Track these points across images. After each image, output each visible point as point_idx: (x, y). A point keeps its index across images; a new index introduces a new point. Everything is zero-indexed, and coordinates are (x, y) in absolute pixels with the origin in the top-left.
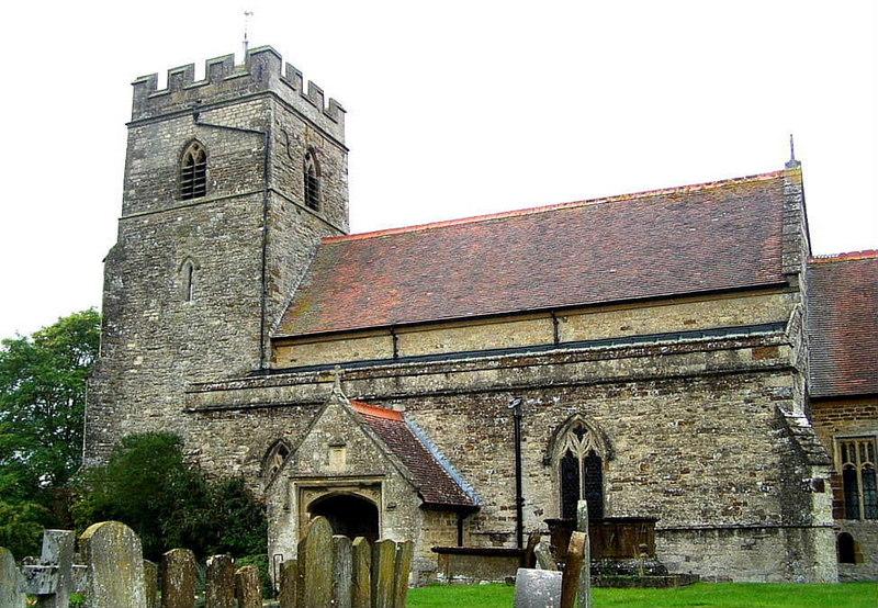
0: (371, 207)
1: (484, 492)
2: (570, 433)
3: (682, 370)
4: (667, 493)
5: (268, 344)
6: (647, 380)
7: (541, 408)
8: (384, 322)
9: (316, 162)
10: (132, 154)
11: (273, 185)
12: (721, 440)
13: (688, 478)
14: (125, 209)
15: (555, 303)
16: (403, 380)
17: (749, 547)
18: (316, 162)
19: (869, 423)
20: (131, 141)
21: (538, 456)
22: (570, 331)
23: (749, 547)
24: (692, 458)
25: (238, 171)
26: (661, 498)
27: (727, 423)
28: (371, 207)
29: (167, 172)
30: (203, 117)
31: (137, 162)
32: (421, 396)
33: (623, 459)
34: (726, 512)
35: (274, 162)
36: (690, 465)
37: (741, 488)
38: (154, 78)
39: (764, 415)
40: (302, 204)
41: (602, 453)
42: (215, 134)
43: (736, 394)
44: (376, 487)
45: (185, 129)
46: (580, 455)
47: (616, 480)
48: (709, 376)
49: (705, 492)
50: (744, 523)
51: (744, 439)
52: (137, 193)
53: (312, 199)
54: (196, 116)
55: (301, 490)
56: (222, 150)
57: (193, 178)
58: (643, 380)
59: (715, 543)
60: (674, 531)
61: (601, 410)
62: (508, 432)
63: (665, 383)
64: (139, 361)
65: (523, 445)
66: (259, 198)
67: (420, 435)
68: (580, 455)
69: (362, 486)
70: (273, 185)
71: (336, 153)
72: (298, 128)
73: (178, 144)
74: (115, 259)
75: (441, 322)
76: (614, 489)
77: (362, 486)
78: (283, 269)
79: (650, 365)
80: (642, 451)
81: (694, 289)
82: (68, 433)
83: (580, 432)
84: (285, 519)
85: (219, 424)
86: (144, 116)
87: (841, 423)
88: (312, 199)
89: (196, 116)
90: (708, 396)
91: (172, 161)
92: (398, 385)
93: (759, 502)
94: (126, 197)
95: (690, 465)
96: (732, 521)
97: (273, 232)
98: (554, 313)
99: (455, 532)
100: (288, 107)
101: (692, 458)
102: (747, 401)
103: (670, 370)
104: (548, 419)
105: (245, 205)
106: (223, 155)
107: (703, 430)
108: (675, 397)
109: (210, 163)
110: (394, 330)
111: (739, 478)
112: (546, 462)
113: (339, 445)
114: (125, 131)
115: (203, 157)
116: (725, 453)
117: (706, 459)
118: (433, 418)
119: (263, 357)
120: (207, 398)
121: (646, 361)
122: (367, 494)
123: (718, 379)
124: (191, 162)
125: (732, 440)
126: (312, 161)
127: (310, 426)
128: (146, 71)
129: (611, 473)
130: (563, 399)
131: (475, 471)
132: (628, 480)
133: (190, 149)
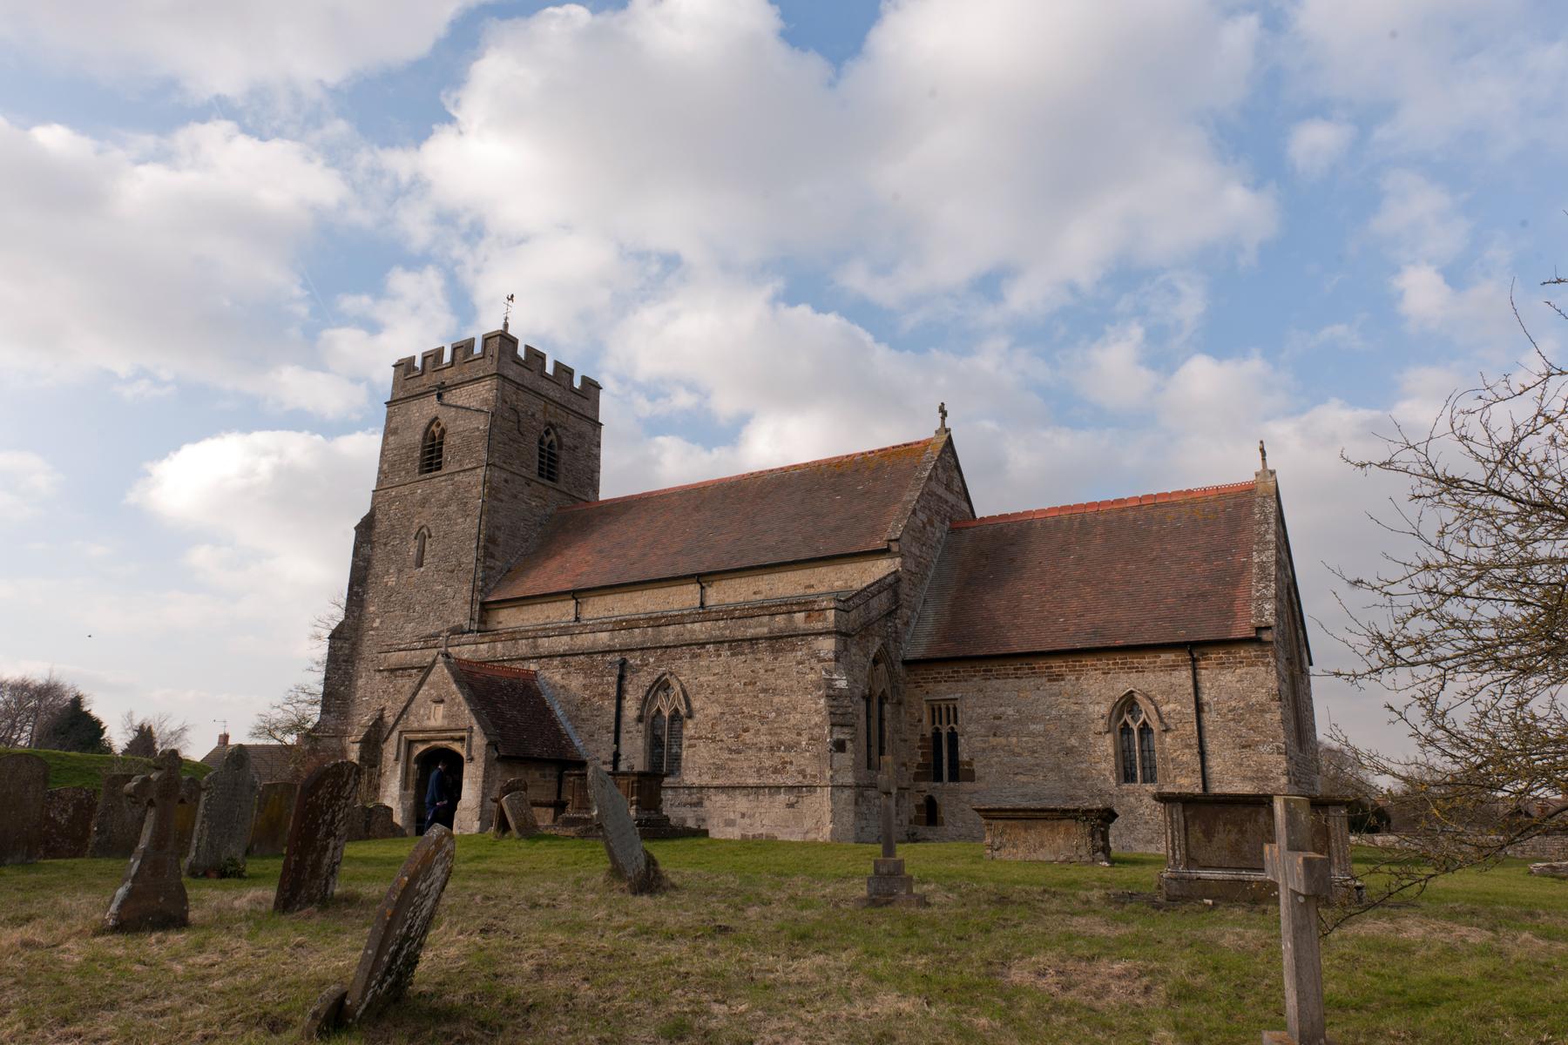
1: (592, 746)
3: (750, 633)
4: (730, 751)
8: (570, 587)
9: (559, 437)
13: (747, 737)
14: (380, 482)
15: (702, 569)
16: (540, 641)
17: (791, 806)
18: (559, 437)
19: (953, 685)
20: (389, 419)
23: (791, 806)
24: (752, 717)
26: (726, 755)
27: (782, 683)
29: (412, 449)
30: (447, 397)
31: (391, 439)
32: (550, 656)
34: (776, 771)
37: (789, 748)
38: (440, 352)
39: (812, 677)
40: (535, 476)
41: (683, 711)
42: (453, 412)
43: (790, 656)
45: (430, 407)
47: (692, 738)
48: (770, 638)
49: (760, 749)
51: (798, 697)
54: (440, 396)
58: (719, 642)
59: (765, 800)
60: (734, 788)
62: (613, 691)
63: (735, 645)
64: (377, 624)
69: (453, 739)
72: (537, 406)
73: (425, 422)
75: (660, 580)
76: (690, 746)
77: (453, 739)
79: (726, 628)
80: (714, 710)
81: (813, 554)
84: (394, 771)
85: (400, 681)
86: (401, 395)
87: (931, 686)
90: (768, 658)
91: (419, 437)
92: (536, 647)
93: (803, 761)
98: (702, 578)
99: (553, 785)
101: (752, 717)
102: (799, 663)
107: (765, 691)
108: (743, 658)
110: (577, 594)
111: (788, 737)
112: (640, 719)
114: (385, 409)
115: (443, 431)
116: (779, 712)
117: (763, 719)
118: (558, 677)
121: (721, 623)
122: (456, 747)
123: (779, 641)
125: (785, 700)
126: (553, 436)
127: (421, 684)
128: (406, 355)
129: (690, 729)
130: (657, 659)
132: (700, 738)
133: (434, 428)
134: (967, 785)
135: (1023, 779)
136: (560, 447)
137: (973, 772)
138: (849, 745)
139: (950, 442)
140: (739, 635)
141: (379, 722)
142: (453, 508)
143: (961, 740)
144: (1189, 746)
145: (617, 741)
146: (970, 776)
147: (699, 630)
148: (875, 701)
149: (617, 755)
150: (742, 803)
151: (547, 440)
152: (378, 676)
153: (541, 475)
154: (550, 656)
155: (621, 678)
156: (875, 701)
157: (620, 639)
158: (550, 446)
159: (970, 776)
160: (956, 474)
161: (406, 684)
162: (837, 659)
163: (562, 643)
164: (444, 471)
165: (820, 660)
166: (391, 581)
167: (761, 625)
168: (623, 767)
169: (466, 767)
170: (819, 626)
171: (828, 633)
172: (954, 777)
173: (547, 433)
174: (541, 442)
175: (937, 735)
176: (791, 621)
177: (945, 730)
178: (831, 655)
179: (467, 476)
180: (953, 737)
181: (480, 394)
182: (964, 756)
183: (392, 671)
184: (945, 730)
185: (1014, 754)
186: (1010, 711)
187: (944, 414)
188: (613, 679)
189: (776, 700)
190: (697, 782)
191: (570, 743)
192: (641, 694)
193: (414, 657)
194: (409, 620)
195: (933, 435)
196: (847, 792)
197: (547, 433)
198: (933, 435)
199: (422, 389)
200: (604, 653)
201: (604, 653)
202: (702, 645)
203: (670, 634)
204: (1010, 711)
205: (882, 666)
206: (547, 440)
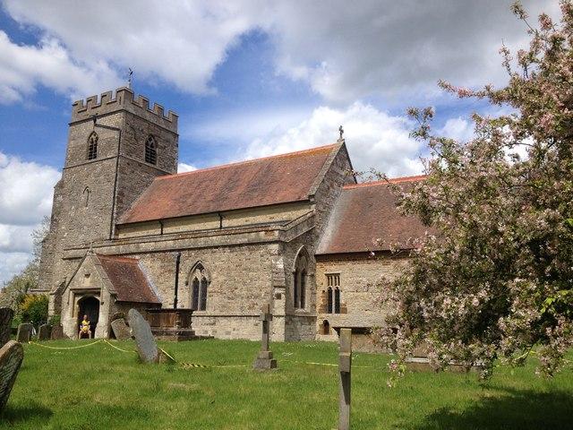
5: (114, 227)
21: (185, 280)
22: (226, 223)
26: (226, 300)
28: (59, 176)
32: (146, 253)
33: (213, 282)
34: (250, 308)
37: (256, 297)
42: (101, 129)
61: (208, 259)
62: (175, 269)
65: (179, 275)
66: (115, 159)
68: (200, 280)
71: (170, 137)
73: (88, 134)
80: (221, 279)
90: (247, 253)
98: (221, 215)
102: (262, 256)
108: (235, 253)
111: (256, 292)
117: (244, 283)
119: (111, 233)
124: (92, 142)
127: (80, 266)
133: (93, 136)
134: (343, 315)
135: (370, 313)
136: (157, 146)
137: (346, 309)
138: (283, 296)
139: (344, 145)
140: (234, 242)
141: (62, 285)
142: (102, 177)
143: (341, 294)
144: (170, 271)
145: (176, 294)
146: (345, 311)
147: (216, 240)
148: (300, 274)
149: (176, 301)
150: (234, 323)
151: (150, 143)
152: (64, 262)
153: (147, 161)
154: (146, 253)
155: (178, 263)
156: (300, 274)
157: (179, 244)
158: (152, 146)
159: (345, 311)
160: (347, 162)
161: (75, 264)
162: (279, 254)
163: (151, 246)
164: (98, 159)
165: (272, 255)
166: (375, 413)
167: (245, 237)
168: (179, 307)
169: (101, 306)
170: (270, 238)
171: (275, 242)
172: (338, 311)
173: (150, 139)
174: (147, 144)
175: (330, 291)
176: (258, 235)
177: (334, 288)
178: (276, 252)
179: (107, 164)
180: (337, 292)
181: (116, 120)
182: (342, 302)
183: (70, 259)
184: (334, 288)
185: (365, 299)
186: (364, 280)
187: (342, 132)
188: (175, 263)
189: (251, 273)
190: (213, 314)
191: (154, 295)
192: (188, 271)
193: (80, 253)
194: (81, 233)
195: (336, 142)
196: (282, 318)
197: (150, 139)
198: (336, 142)
199: (88, 117)
200: (171, 251)
201: (171, 251)
202: (217, 247)
203: (201, 242)
204: (364, 280)
205: (304, 258)
206: (150, 143)
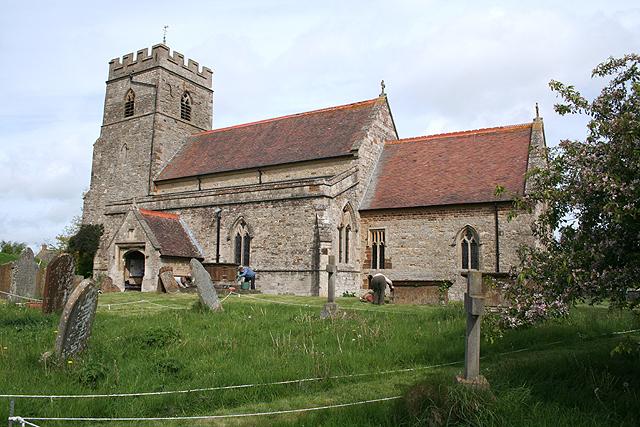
0: (221, 121)
2: (239, 225)
3: (282, 197)
6: (268, 201)
7: (228, 214)
8: (195, 173)
10: (108, 96)
11: (159, 109)
12: (294, 229)
15: (260, 164)
17: (302, 280)
22: (266, 178)
23: (302, 280)
25: (146, 102)
26: (270, 256)
29: (120, 104)
33: (257, 238)
35: (160, 99)
36: (282, 241)
43: (302, 208)
44: (144, 248)
46: (242, 235)
50: (301, 269)
52: (109, 114)
53: (186, 113)
55: (121, 248)
56: (141, 93)
57: (129, 109)
61: (250, 214)
67: (185, 226)
68: (242, 235)
70: (159, 109)
71: (205, 93)
74: (98, 144)
78: (163, 149)
82: (609, 270)
83: (243, 224)
88: (186, 113)
89: (131, 78)
90: (291, 208)
94: (104, 117)
95: (282, 241)
96: (296, 268)
97: (157, 131)
98: (260, 170)
100: (171, 72)
103: (277, 197)
104: (231, 219)
105: (147, 119)
106: (147, 91)
107: (288, 225)
108: (278, 209)
109: (136, 100)
113: (132, 230)
116: (295, 235)
120: (113, 208)
121: (268, 192)
123: (295, 200)
126: (188, 97)
131: (203, 242)
133: (129, 94)
